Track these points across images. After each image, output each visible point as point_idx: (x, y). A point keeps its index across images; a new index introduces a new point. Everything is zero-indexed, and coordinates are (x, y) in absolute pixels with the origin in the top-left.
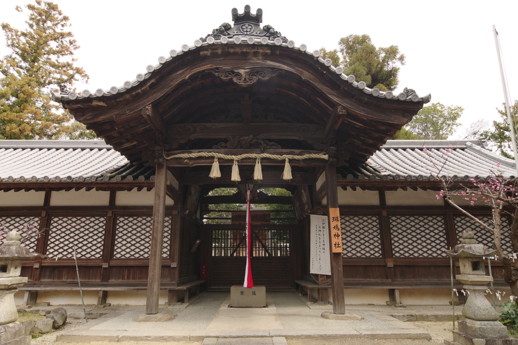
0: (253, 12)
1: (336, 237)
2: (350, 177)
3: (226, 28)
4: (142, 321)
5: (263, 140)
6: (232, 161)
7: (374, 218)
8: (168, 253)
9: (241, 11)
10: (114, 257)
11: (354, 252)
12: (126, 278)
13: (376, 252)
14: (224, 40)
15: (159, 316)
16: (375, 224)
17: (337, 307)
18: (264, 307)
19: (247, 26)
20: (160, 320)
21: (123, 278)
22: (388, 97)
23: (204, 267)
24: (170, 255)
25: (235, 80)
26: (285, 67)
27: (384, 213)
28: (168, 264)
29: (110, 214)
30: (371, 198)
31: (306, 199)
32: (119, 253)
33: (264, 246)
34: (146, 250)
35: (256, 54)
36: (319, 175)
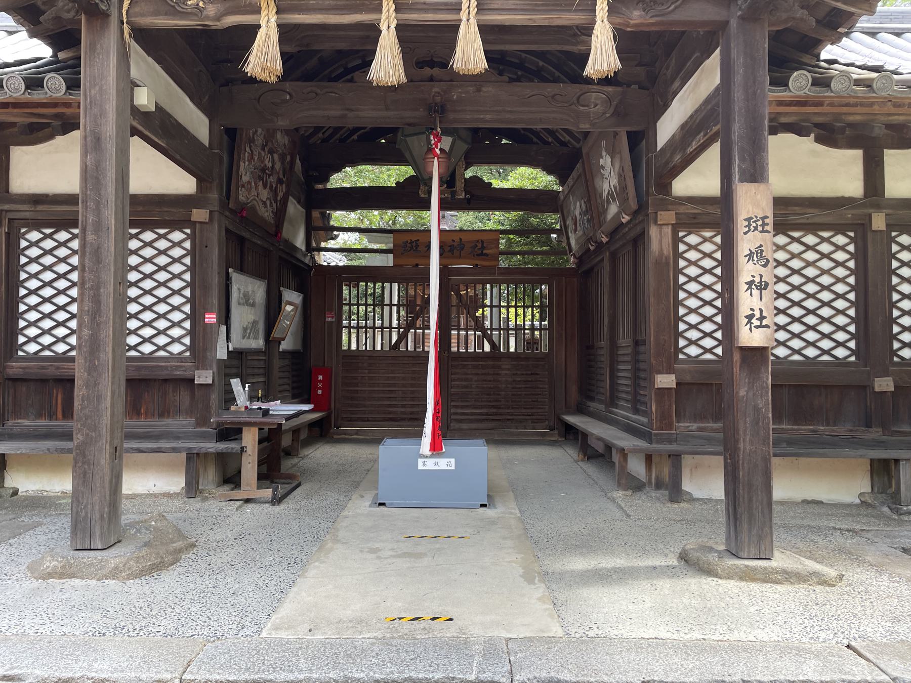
1: (756, 292)
4: (50, 575)
7: (841, 240)
8: (187, 341)
10: (21, 353)
12: (60, 415)
13: (839, 344)
15: (114, 557)
16: (840, 256)
17: (744, 536)
18: (483, 506)
20: (114, 574)
21: (51, 416)
23: (321, 377)
24: (192, 348)
27: (879, 222)
28: (187, 374)
31: (614, 181)
32: (34, 339)
33: (479, 325)
36: (677, 84)
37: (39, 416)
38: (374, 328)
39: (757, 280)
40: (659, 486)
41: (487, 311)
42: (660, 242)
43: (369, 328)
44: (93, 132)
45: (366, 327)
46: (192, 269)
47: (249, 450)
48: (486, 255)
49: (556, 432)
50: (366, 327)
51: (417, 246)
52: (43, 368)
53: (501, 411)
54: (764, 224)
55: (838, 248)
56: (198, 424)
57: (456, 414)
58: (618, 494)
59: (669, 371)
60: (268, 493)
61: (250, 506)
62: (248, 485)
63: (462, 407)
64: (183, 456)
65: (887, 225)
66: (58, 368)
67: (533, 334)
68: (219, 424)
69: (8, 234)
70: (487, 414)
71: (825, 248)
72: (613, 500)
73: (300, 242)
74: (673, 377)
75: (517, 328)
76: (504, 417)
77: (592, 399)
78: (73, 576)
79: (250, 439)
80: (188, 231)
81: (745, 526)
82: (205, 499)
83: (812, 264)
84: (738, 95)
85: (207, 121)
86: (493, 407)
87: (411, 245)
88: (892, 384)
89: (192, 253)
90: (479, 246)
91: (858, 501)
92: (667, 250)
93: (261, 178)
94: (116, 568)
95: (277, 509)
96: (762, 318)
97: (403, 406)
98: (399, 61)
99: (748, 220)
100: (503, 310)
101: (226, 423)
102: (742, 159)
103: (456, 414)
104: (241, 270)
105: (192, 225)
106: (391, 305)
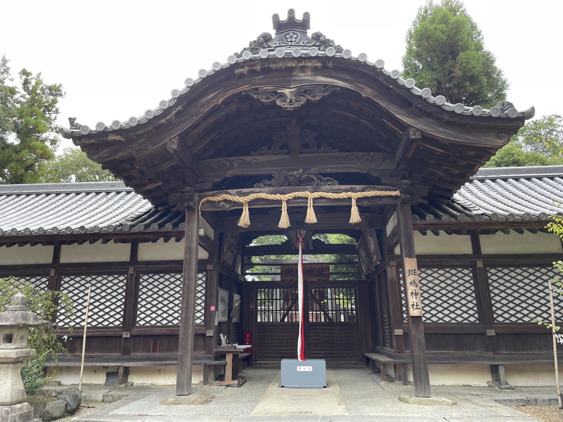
0: (299, 17)
1: (414, 296)
2: (430, 218)
3: (265, 39)
4: (171, 404)
5: (315, 174)
6: (280, 202)
7: (466, 271)
9: (284, 17)
10: (137, 325)
11: (440, 315)
14: (263, 54)
15: (192, 397)
16: (467, 278)
18: (325, 387)
19: (293, 36)
20: (193, 403)
22: (476, 114)
23: (248, 336)
24: (204, 321)
25: (278, 102)
26: (341, 83)
27: (480, 264)
28: (203, 332)
29: (131, 271)
30: (461, 245)
31: (374, 247)
34: (176, 315)
35: (303, 69)
37: (143, 351)
38: (269, 311)
39: (414, 292)
40: (400, 379)
41: (330, 301)
42: (392, 273)
43: (269, 312)
44: (189, 247)
45: (265, 310)
46: (205, 288)
47: (229, 363)
48: (324, 275)
49: (362, 363)
50: (265, 310)
51: (292, 271)
52: (146, 330)
53: (335, 352)
54: (415, 272)
55: (465, 275)
56: (207, 353)
57: (313, 354)
58: (383, 383)
59: (400, 328)
60: (236, 382)
61: (229, 388)
62: (228, 378)
63: (316, 350)
64: (202, 367)
65: (484, 265)
66: (152, 331)
67: (352, 313)
68: (217, 352)
69: (136, 277)
70: (328, 354)
71: (460, 275)
72: (380, 385)
73: (239, 272)
74: (401, 330)
75: (344, 309)
76: (336, 355)
77: (377, 345)
78: (178, 404)
79: (229, 359)
80: (205, 273)
81: (419, 384)
82: (210, 385)
83: (455, 282)
84: (402, 228)
85: (213, 231)
86: (331, 350)
87: (289, 271)
88: (494, 332)
89: (206, 282)
90: (320, 271)
91: (487, 385)
92: (395, 277)
93: (229, 249)
94: (194, 400)
95: (240, 389)
96: (417, 306)
97: (287, 350)
98: (288, 220)
99: (409, 271)
100: (337, 301)
101: (220, 352)
102: (406, 250)
103: (313, 354)
104: (221, 287)
105: (207, 271)
106: (276, 299)
